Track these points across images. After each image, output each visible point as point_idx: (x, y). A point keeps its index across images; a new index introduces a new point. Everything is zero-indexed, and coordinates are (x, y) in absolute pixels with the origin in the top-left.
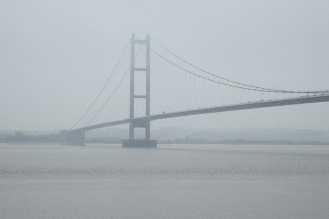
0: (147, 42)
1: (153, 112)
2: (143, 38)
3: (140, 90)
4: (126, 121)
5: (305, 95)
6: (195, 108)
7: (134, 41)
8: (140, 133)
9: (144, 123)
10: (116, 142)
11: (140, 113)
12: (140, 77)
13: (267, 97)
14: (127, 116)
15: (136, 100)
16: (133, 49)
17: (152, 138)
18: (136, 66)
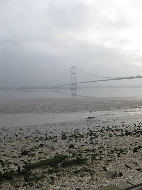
0: (75, 68)
1: (76, 82)
2: (74, 67)
3: (74, 77)
4: (71, 84)
5: (112, 78)
6: (82, 82)
7: (72, 68)
8: (74, 87)
9: (75, 84)
10: (68, 88)
11: (74, 82)
12: (74, 75)
13: (108, 79)
14: (71, 83)
15: (74, 73)
16: (72, 75)
17: (76, 87)
18: (73, 73)
